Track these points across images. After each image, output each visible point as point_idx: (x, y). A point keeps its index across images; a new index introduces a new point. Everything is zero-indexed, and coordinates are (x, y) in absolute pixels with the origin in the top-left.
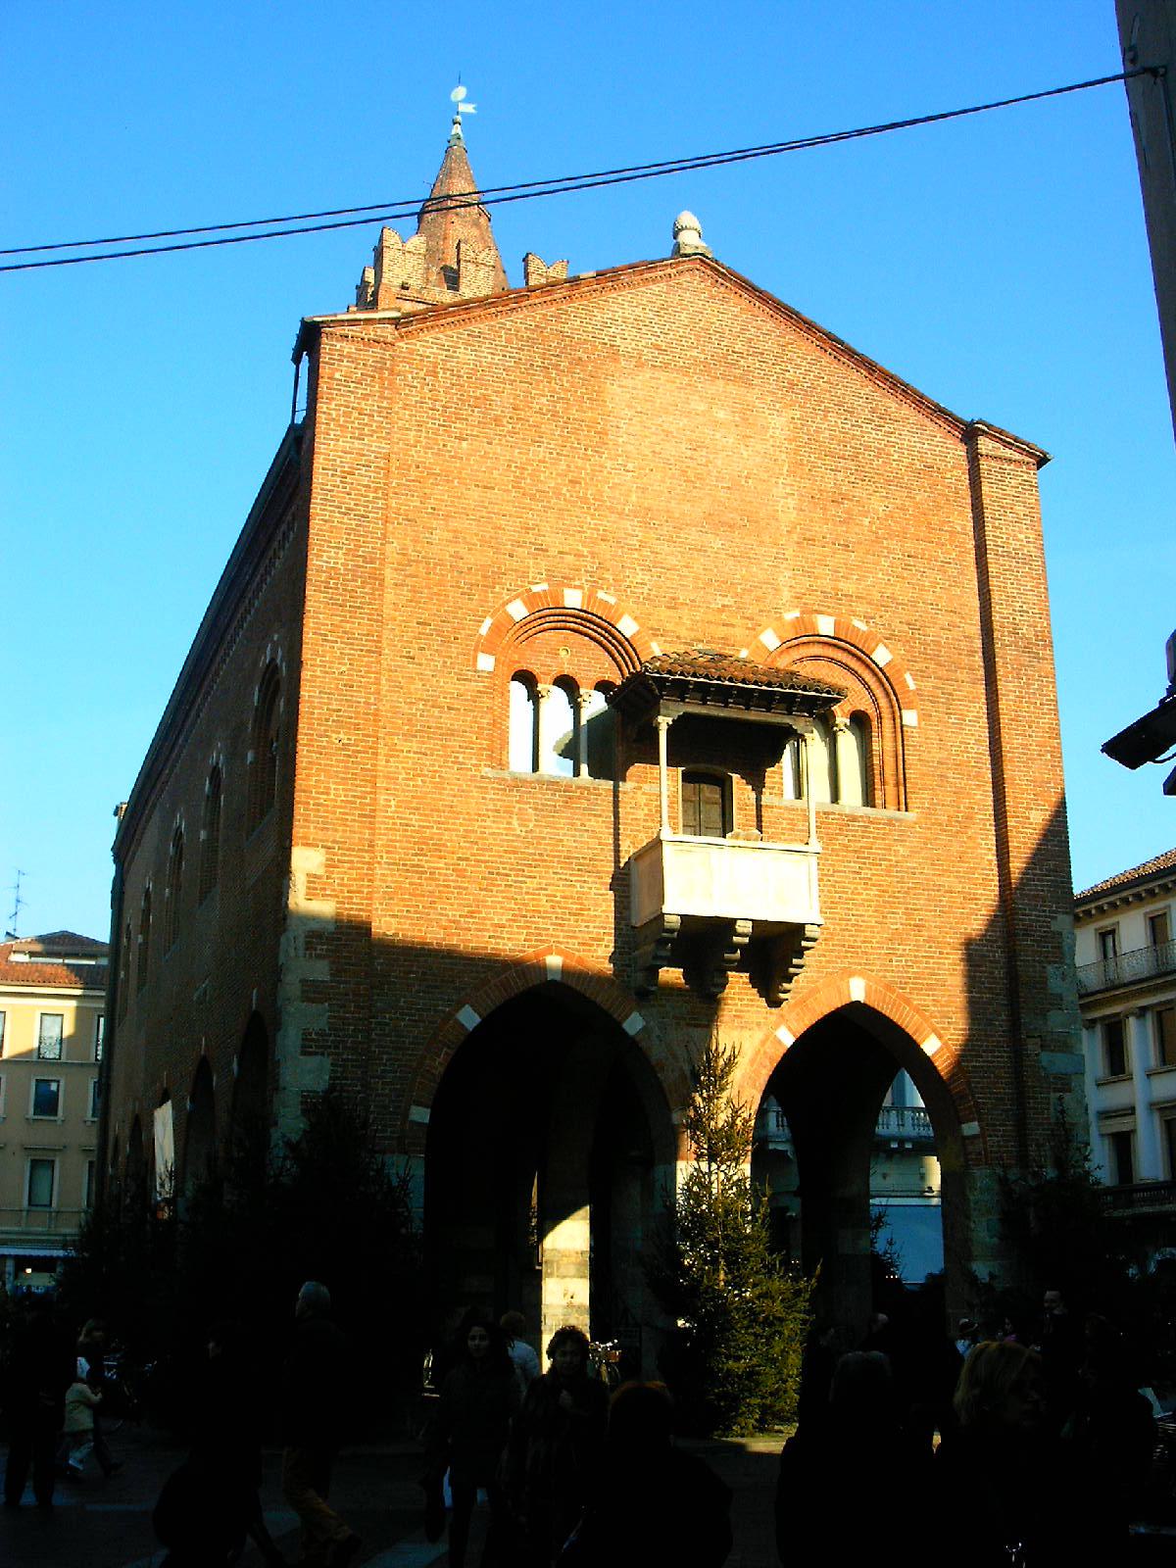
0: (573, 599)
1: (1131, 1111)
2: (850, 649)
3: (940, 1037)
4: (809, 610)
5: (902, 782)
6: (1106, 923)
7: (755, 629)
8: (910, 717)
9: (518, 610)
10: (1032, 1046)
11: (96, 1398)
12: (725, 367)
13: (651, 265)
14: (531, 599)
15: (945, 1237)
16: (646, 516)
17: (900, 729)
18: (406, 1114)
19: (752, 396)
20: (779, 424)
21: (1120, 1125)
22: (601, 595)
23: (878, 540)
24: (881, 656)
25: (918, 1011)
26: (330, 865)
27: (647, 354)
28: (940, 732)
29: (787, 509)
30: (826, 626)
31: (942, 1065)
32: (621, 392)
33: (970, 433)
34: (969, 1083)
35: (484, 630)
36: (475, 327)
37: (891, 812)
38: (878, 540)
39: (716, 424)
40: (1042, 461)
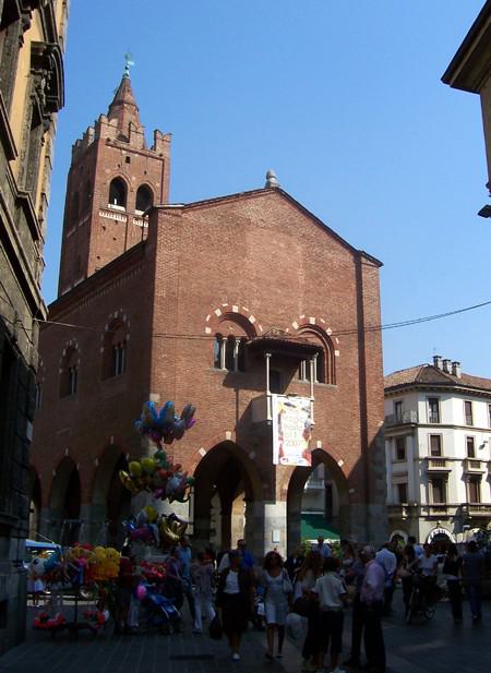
0: (235, 309)
1: (406, 474)
2: (318, 330)
5: (333, 375)
6: (398, 398)
7: (291, 322)
8: (337, 353)
9: (218, 313)
10: (371, 465)
11: (310, 572)
12: (282, 229)
13: (258, 191)
14: (222, 309)
15: (88, 255)
16: (258, 280)
17: (333, 357)
19: (292, 239)
20: (299, 249)
21: (402, 480)
23: (329, 291)
24: (329, 331)
27: (260, 223)
28: (344, 356)
29: (302, 279)
30: (312, 321)
31: (347, 473)
32: (251, 238)
33: (358, 255)
35: (208, 319)
36: (205, 210)
37: (330, 385)
38: (329, 291)
39: (280, 248)
40: (381, 265)
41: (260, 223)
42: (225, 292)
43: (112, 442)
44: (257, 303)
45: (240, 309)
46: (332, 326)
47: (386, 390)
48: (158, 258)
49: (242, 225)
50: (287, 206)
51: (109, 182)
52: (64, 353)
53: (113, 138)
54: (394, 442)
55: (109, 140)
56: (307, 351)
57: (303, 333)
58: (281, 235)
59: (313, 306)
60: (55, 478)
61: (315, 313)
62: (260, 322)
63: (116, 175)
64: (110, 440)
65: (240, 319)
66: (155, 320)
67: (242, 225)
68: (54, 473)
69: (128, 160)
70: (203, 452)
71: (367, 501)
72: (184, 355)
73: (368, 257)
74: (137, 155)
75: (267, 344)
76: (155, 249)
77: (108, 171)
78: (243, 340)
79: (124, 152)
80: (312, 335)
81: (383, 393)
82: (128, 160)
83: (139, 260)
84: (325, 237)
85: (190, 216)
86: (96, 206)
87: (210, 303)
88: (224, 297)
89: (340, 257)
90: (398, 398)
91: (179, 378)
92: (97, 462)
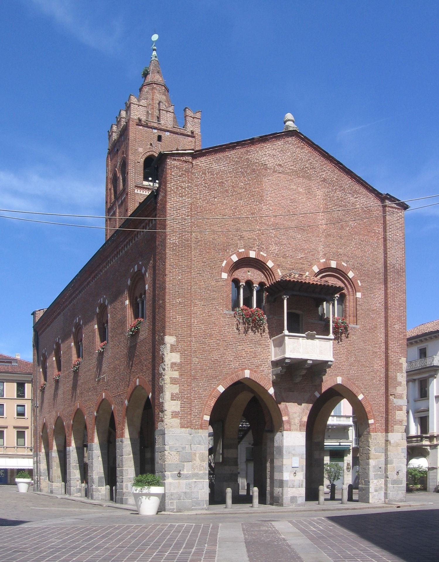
3: (363, 395)
4: (328, 259)
6: (422, 345)
7: (311, 265)
12: (303, 173)
14: (238, 254)
18: (202, 418)
20: (320, 193)
21: (423, 415)
22: (261, 253)
25: (357, 387)
26: (178, 341)
27: (277, 168)
32: (268, 182)
34: (371, 408)
35: (224, 265)
41: (277, 168)
42: (242, 237)
43: (138, 384)
44: (274, 248)
45: (258, 254)
46: (353, 269)
47: (408, 339)
48: (168, 206)
49: (258, 171)
50: (307, 149)
51: (142, 160)
52: (98, 310)
53: (144, 118)
54: (417, 383)
55: (140, 120)
56: (326, 293)
57: (321, 278)
58: (301, 180)
59: (334, 250)
60: (96, 417)
61: (337, 256)
62: (279, 266)
63: (148, 154)
64: (136, 383)
65: (258, 264)
66: (168, 266)
67: (258, 171)
68: (95, 414)
69: (159, 138)
70: (221, 389)
71: (387, 431)
72: (201, 300)
73: (392, 199)
74: (168, 134)
75: (284, 287)
76: (165, 197)
77: (141, 150)
78: (261, 284)
79: (156, 131)
80: (332, 278)
81: (405, 342)
82: (159, 138)
83: (153, 205)
84: (347, 181)
85: (202, 162)
86: (131, 184)
87: (225, 249)
88: (241, 243)
89: (363, 200)
90: (422, 345)
91: (195, 321)
92: (126, 402)
